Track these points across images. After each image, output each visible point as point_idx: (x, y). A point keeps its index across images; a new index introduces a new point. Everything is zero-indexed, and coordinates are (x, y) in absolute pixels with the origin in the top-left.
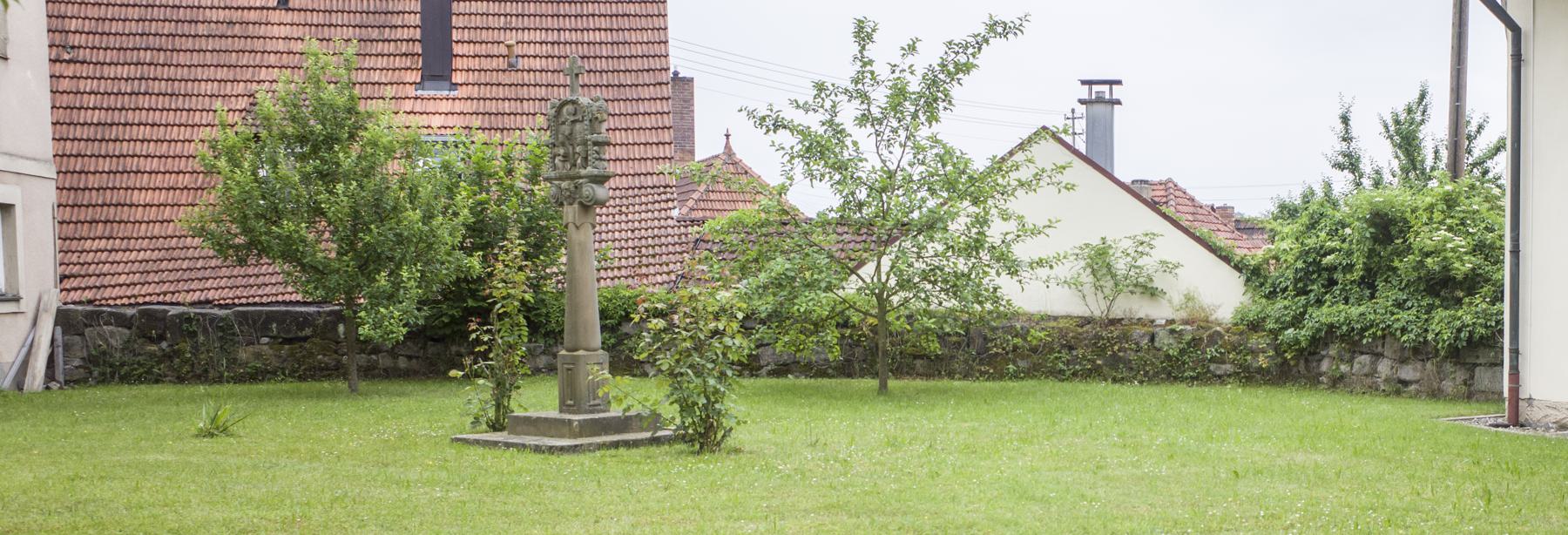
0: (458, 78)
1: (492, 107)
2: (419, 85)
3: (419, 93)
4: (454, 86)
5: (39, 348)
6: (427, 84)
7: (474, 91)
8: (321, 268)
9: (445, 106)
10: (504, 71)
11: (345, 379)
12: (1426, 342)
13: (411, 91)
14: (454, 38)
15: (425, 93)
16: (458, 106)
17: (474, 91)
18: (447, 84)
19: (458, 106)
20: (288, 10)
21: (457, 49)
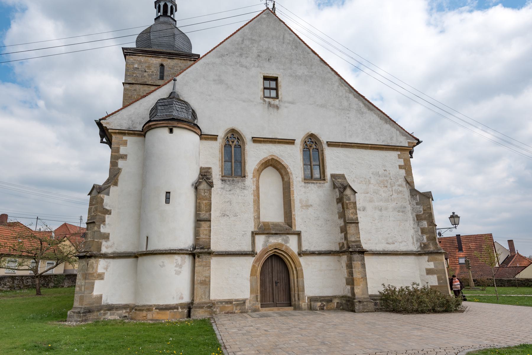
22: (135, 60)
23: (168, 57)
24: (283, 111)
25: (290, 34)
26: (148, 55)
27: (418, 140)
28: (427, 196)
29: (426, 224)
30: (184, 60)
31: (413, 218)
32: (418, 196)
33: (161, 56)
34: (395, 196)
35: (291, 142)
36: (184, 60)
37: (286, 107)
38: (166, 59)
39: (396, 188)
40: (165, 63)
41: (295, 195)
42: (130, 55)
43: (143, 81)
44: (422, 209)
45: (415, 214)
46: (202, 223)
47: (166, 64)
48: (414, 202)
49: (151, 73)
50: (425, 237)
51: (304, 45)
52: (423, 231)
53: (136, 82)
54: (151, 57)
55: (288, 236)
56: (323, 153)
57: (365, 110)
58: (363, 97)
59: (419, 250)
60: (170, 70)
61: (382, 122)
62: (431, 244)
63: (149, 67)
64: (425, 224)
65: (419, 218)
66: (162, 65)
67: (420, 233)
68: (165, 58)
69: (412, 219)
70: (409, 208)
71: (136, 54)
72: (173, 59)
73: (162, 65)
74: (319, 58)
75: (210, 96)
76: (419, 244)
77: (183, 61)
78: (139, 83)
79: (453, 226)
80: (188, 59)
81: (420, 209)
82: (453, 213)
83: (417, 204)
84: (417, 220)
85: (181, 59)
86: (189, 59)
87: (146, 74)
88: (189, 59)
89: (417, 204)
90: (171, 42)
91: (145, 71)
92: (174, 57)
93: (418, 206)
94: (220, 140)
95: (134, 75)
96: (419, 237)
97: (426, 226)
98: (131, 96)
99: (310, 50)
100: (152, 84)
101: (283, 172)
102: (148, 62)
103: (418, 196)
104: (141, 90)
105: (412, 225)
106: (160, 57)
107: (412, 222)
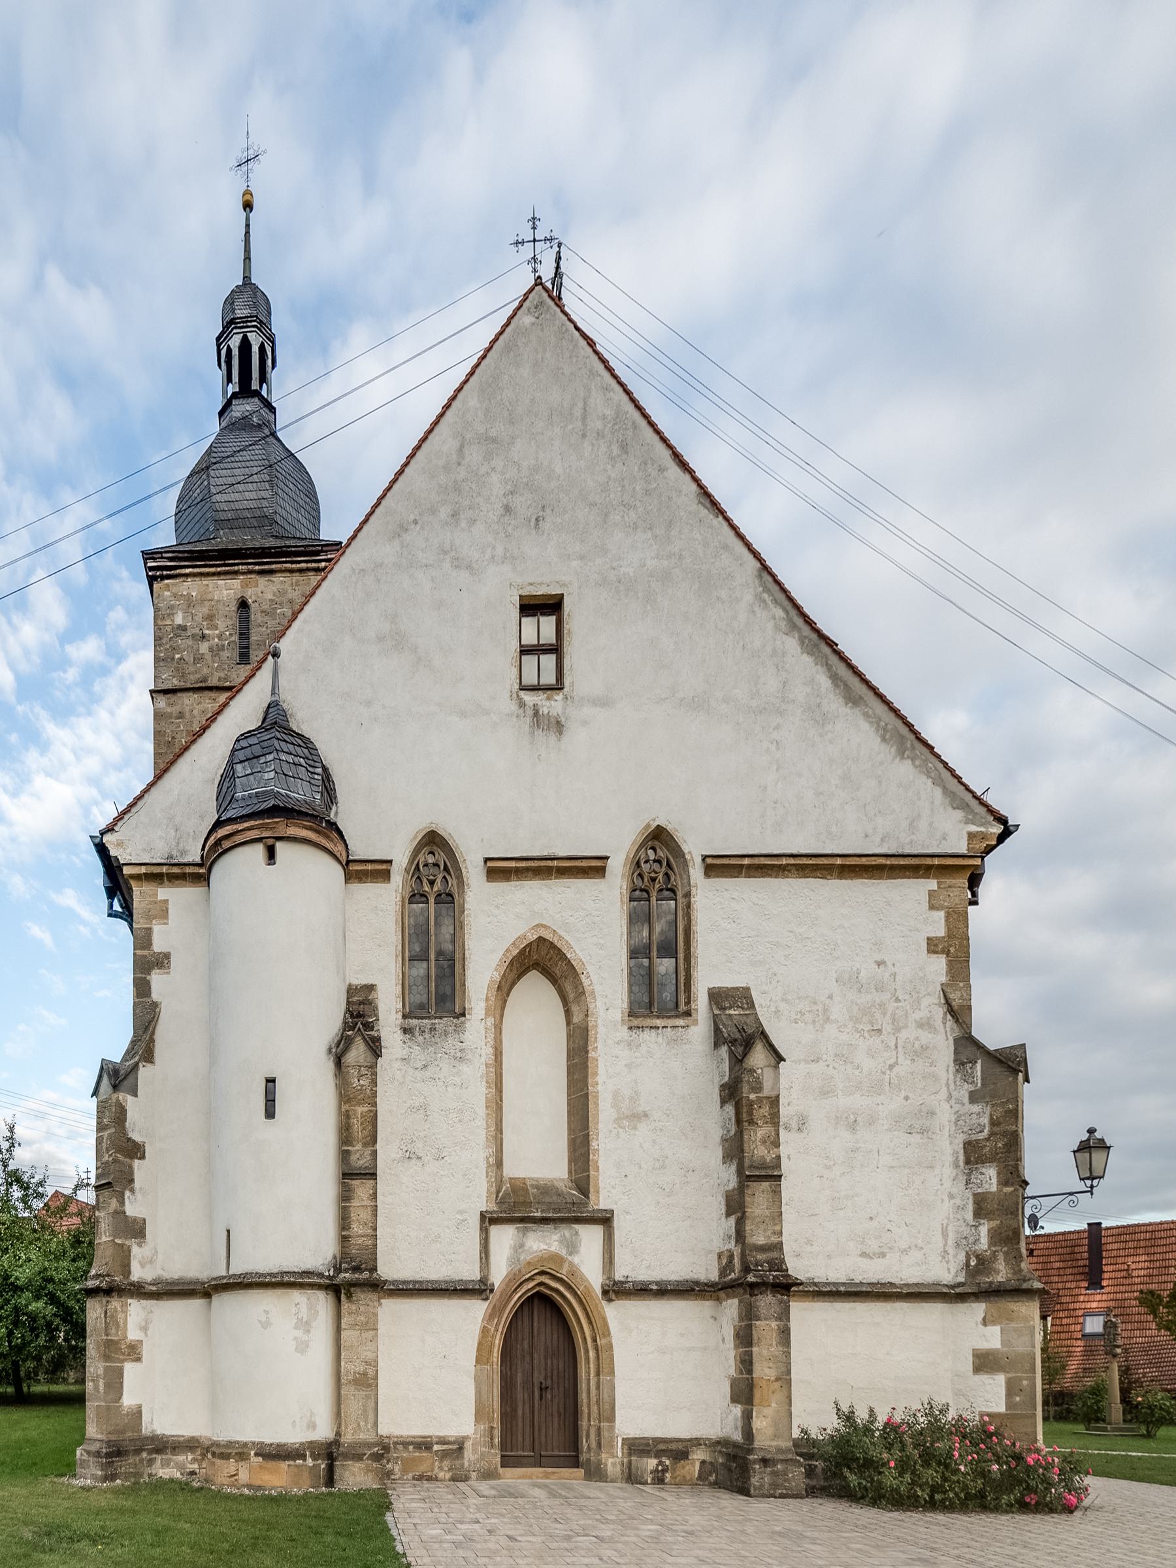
0: (1104, 1283)
1: (1119, 1296)
2: (1087, 1289)
3: (1087, 1291)
4: (1102, 1287)
5: (582, 1414)
6: (1091, 1287)
7: (1112, 1289)
8: (824, 660)
9: (1098, 1297)
10: (1126, 1278)
11: (350, 985)
12: (932, 1485)
13: (1083, 1291)
14: (1104, 1256)
15: (1089, 1292)
16: (1105, 1297)
17: (1112, 1289)
18: (1099, 1287)
19: (1105, 1297)
20: (1033, 1256)
21: (1105, 1268)
22: (175, 595)
23: (257, 567)
24: (577, 737)
25: (607, 389)
26: (212, 570)
27: (1002, 820)
28: (136, 1151)
29: (994, 1181)
30: (301, 571)
31: (956, 1153)
32: (979, 1066)
33: (240, 567)
34: (905, 1066)
35: (593, 867)
36: (301, 571)
37: (585, 723)
38: (253, 576)
39: (909, 1033)
40: (250, 595)
41: (601, 1079)
42: (163, 578)
43: (197, 676)
44: (985, 1120)
45: (961, 1139)
46: (355, 1183)
47: (254, 598)
48: (964, 1092)
49: (216, 640)
50: (984, 1230)
51: (648, 432)
52: (982, 1207)
53: (182, 685)
54: (214, 574)
55: (576, 1227)
56: (689, 906)
57: (834, 703)
58: (831, 644)
59: (961, 1279)
60: (266, 619)
61: (885, 752)
62: (1001, 1257)
63: (210, 618)
64: (990, 1178)
65: (973, 1154)
66: (243, 605)
67: (969, 1215)
68: (250, 572)
69: (949, 1159)
70: (945, 1115)
71: (178, 571)
72: (271, 572)
73: (243, 605)
74: (694, 487)
75: (369, 703)
76: (962, 1257)
77: (296, 577)
78: (189, 686)
79: (1081, 1186)
80: (309, 565)
81: (981, 1116)
82: (1091, 1131)
83: (974, 1098)
84: (967, 1162)
85: (291, 571)
86: (314, 565)
87: (204, 647)
88: (314, 565)
89: (974, 1098)
90: (265, 503)
91: (203, 636)
92: (273, 566)
93: (976, 1108)
94: (398, 877)
95: (177, 656)
96: (966, 1231)
97: (994, 1189)
98: (173, 738)
99: (666, 453)
100: (220, 684)
101: (569, 988)
102: (209, 597)
103: (979, 1066)
104: (195, 712)
105: (948, 1184)
106: (236, 573)
107: (948, 1172)
